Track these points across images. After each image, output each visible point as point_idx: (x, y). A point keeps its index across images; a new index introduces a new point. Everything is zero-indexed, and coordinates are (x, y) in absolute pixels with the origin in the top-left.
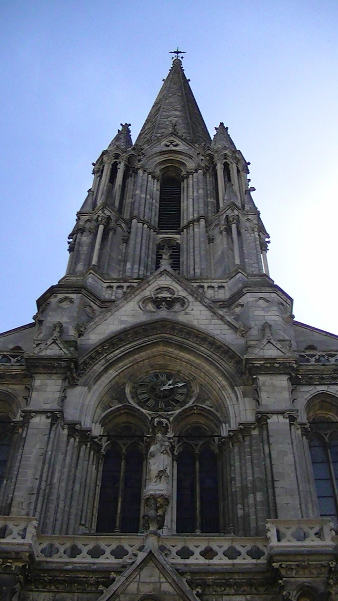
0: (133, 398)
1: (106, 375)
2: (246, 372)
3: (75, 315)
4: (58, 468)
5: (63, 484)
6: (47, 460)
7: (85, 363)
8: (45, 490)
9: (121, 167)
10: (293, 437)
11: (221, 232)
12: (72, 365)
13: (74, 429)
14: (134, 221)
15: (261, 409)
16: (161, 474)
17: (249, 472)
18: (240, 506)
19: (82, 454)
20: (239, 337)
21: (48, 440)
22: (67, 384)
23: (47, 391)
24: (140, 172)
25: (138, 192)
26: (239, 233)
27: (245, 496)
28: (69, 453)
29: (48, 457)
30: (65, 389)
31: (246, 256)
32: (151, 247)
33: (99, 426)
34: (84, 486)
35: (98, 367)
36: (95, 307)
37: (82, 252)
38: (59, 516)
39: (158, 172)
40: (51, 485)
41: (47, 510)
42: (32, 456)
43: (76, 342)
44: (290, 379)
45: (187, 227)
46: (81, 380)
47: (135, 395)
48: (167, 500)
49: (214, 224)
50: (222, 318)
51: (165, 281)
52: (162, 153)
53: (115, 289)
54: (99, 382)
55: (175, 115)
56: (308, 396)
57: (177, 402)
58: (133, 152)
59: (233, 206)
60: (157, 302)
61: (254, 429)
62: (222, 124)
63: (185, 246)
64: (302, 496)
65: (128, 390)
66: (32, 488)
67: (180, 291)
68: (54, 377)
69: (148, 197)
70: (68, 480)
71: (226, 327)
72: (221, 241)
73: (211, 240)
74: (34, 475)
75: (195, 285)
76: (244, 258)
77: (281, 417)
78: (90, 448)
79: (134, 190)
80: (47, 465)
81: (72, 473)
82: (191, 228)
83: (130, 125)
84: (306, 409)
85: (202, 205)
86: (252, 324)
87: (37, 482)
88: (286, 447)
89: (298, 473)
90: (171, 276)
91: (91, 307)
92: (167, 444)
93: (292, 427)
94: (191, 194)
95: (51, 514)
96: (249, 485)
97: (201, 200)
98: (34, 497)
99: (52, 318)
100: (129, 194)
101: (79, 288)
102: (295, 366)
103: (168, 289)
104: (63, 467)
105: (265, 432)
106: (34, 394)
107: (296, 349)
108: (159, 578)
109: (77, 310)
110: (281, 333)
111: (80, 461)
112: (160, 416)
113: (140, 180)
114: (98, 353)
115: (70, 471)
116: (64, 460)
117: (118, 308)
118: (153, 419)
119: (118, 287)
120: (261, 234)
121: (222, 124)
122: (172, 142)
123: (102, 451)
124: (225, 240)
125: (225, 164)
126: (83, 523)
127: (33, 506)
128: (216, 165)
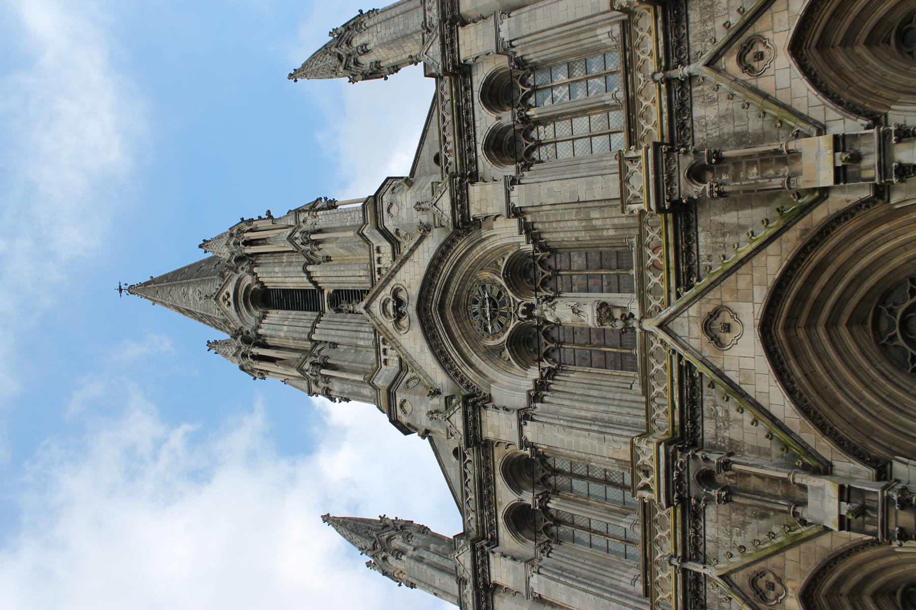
0: (499, 338)
1: (478, 365)
2: (465, 224)
3: (417, 397)
4: (576, 412)
5: (592, 407)
6: (569, 424)
7: (468, 387)
8: (599, 426)
9: (257, 351)
10: (533, 181)
11: (320, 250)
12: (470, 401)
13: (536, 396)
14: (314, 337)
15: (505, 213)
16: (576, 311)
17: (569, 224)
18: (605, 233)
19: (560, 389)
20: (431, 234)
21: (549, 423)
22: (489, 405)
23: (499, 426)
24: (260, 331)
25: (282, 334)
26: (320, 231)
27: (595, 229)
28: (560, 401)
29: (565, 423)
30: (496, 408)
31: (344, 224)
32: (339, 320)
33: (529, 371)
34: (591, 386)
35: (470, 373)
36: (408, 377)
37: (350, 390)
38: (624, 411)
39: (257, 313)
40: (594, 419)
41: (620, 423)
42: (566, 439)
43: (446, 398)
44: (472, 183)
45: (315, 283)
46: (484, 390)
47: (495, 335)
48: (603, 305)
49: (311, 257)
50: (412, 251)
51: (376, 307)
52: (237, 309)
53: (387, 357)
54: (485, 372)
55: (193, 295)
56: (489, 164)
57: (500, 293)
58: (239, 339)
59: (291, 239)
60: (399, 316)
61: (525, 219)
62: (200, 246)
63: (336, 285)
64: (593, 173)
65: (491, 343)
66: (599, 439)
67: (387, 293)
68: (483, 419)
69: (286, 323)
70: (586, 402)
71: (421, 247)
72: (327, 249)
73: (328, 259)
74: (585, 437)
75: (378, 276)
76: (346, 226)
77: (512, 193)
78: (553, 379)
79: (280, 337)
80: (575, 425)
81: (580, 398)
82: (316, 279)
83: (208, 342)
84: (499, 164)
85: (292, 269)
86: (416, 221)
87: (592, 434)
88: (545, 186)
89: (569, 176)
90: (370, 302)
91: (408, 382)
92: (544, 305)
93: (522, 181)
94: (280, 280)
95: (623, 419)
96: (584, 224)
97: (286, 269)
98: (607, 437)
99: (424, 422)
100: (285, 343)
101: (391, 395)
102: (458, 178)
103: (384, 305)
104: (574, 408)
105: (529, 209)
106: (503, 438)
107: (440, 175)
108: (684, 317)
109: (412, 396)
110: (424, 191)
111: (567, 390)
112: (516, 312)
113: (268, 332)
114: (462, 381)
115: (577, 400)
116: (568, 406)
117: (408, 355)
118: (519, 319)
119: (385, 353)
120: (317, 207)
121: (200, 246)
122: (225, 300)
123: (554, 367)
124: (327, 245)
125: (246, 243)
126: (629, 386)
127: (616, 438)
128: (247, 254)
